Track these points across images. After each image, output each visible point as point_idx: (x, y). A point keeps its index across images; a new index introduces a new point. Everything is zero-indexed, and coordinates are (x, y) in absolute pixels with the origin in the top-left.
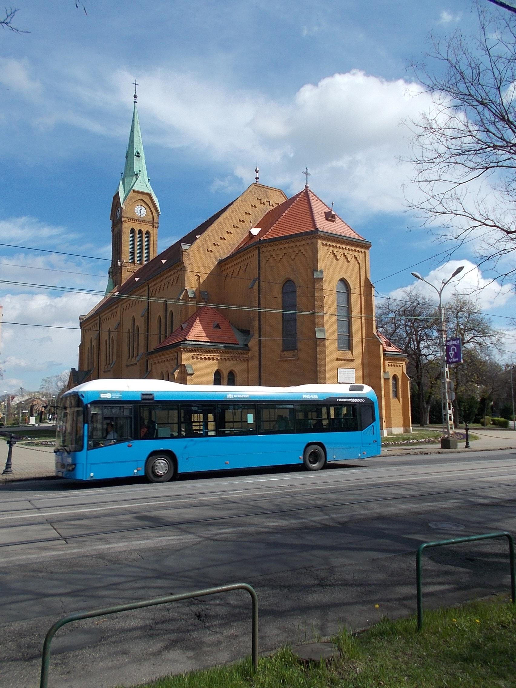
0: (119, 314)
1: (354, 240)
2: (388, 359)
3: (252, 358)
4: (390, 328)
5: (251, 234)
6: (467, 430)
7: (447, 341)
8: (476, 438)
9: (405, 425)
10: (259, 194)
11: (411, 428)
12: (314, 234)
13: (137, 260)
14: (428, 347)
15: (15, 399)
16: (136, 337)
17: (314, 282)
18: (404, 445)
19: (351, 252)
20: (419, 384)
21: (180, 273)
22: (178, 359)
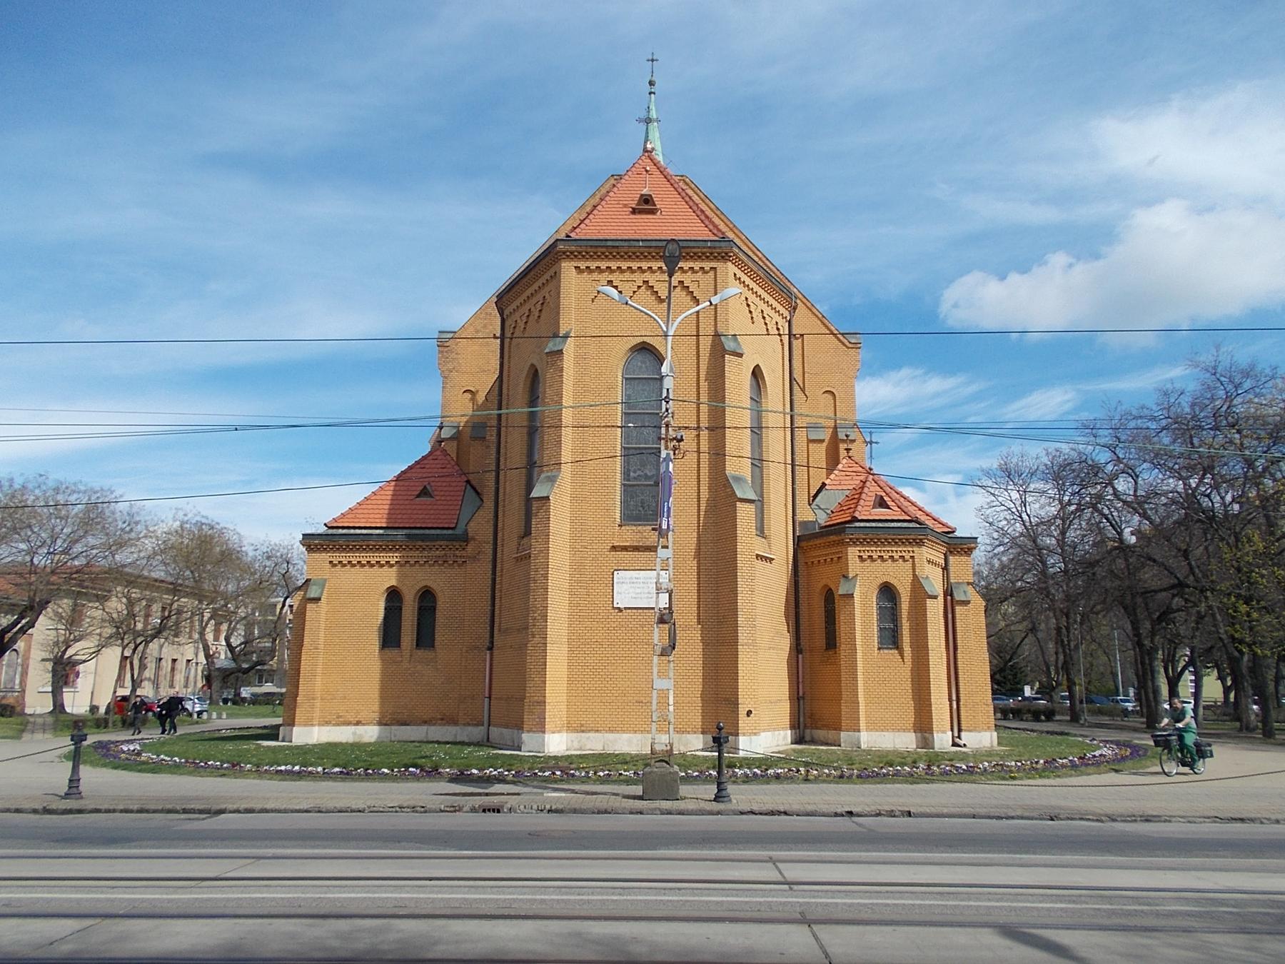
3: (474, 558)
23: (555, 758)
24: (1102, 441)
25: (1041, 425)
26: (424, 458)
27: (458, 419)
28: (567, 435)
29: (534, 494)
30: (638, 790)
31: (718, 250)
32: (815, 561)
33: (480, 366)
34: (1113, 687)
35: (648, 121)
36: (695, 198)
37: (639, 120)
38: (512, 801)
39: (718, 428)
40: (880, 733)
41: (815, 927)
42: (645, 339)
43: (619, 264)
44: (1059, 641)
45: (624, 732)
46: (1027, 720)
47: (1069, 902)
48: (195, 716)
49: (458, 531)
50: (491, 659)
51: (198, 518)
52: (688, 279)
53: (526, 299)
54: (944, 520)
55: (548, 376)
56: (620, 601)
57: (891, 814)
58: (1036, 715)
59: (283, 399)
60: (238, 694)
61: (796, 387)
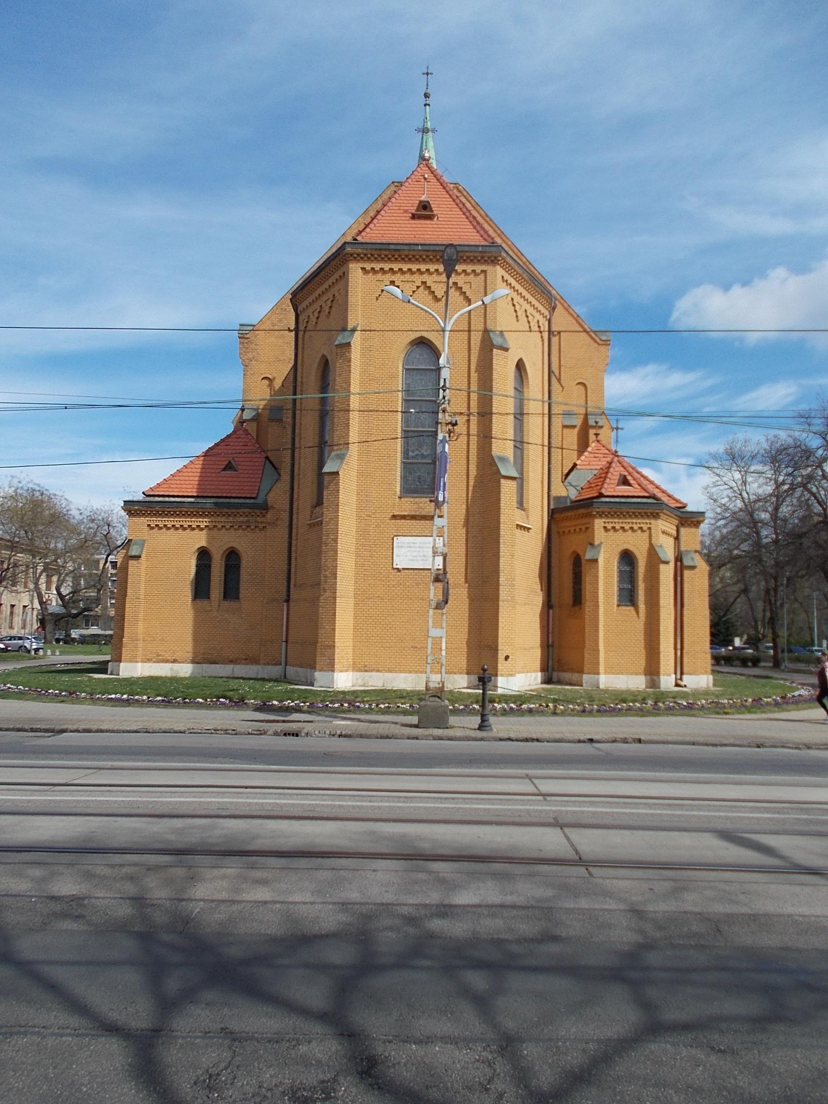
3: (273, 524)
23: (343, 692)
24: (815, 429)
25: (766, 414)
26: (228, 436)
27: (257, 403)
28: (355, 419)
29: (326, 469)
30: (414, 720)
31: (488, 254)
32: (572, 530)
33: (277, 356)
34: (809, 639)
35: (425, 131)
36: (468, 205)
37: (418, 130)
38: (308, 727)
39: (486, 414)
40: (617, 676)
41: (566, 830)
42: (425, 334)
43: (400, 266)
44: (768, 602)
45: (401, 672)
46: (736, 666)
47: (774, 813)
48: (33, 652)
49: (259, 501)
50: (288, 610)
51: (31, 485)
52: (461, 280)
53: (318, 296)
54: (678, 497)
55: (337, 366)
56: (399, 563)
57: (625, 741)
58: (744, 662)
59: (108, 382)
60: (68, 635)
61: (553, 379)
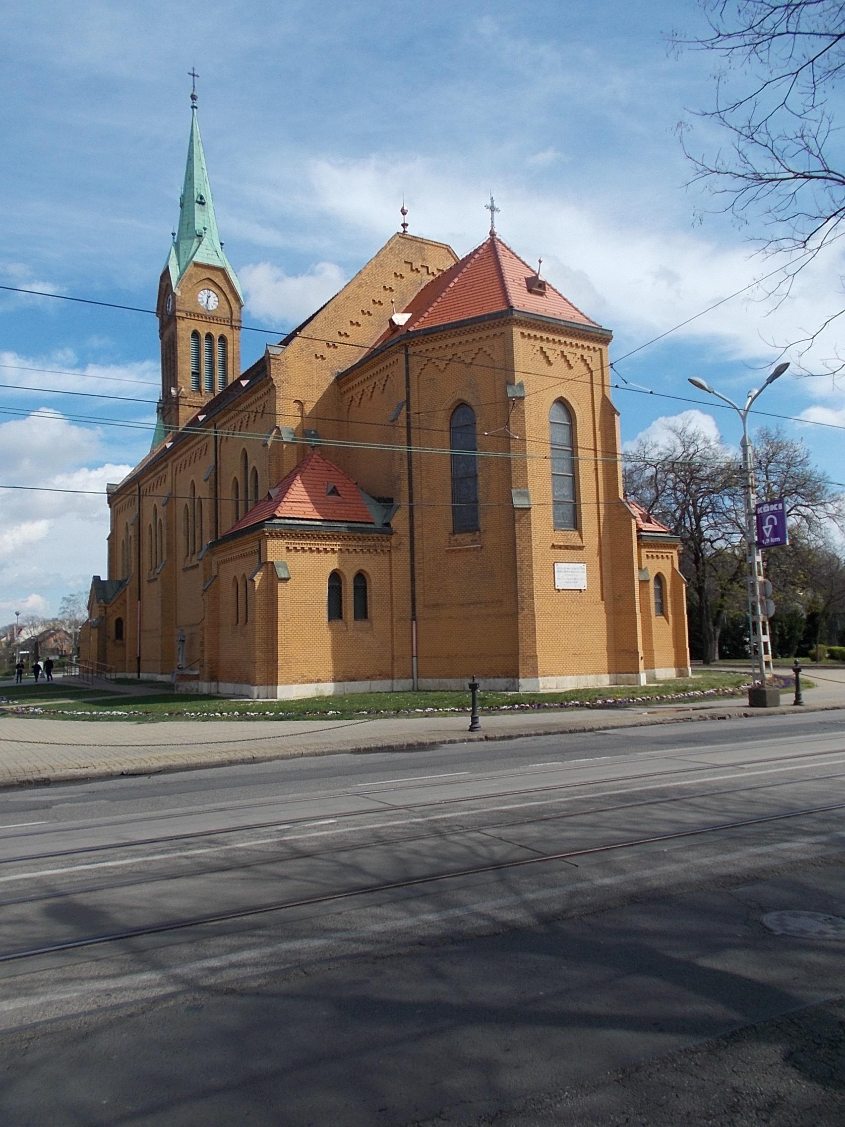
0: (169, 478)
1: (581, 327)
2: (645, 546)
3: (397, 548)
4: (649, 494)
5: (393, 323)
6: (797, 671)
7: (758, 506)
8: (809, 685)
9: (679, 665)
10: (408, 253)
11: (690, 669)
12: (506, 317)
13: (204, 385)
14: (715, 526)
15: (23, 632)
16: (197, 519)
17: (507, 406)
18: (679, 700)
19: (575, 350)
20: (700, 590)
21: (266, 398)
22: (260, 552)
